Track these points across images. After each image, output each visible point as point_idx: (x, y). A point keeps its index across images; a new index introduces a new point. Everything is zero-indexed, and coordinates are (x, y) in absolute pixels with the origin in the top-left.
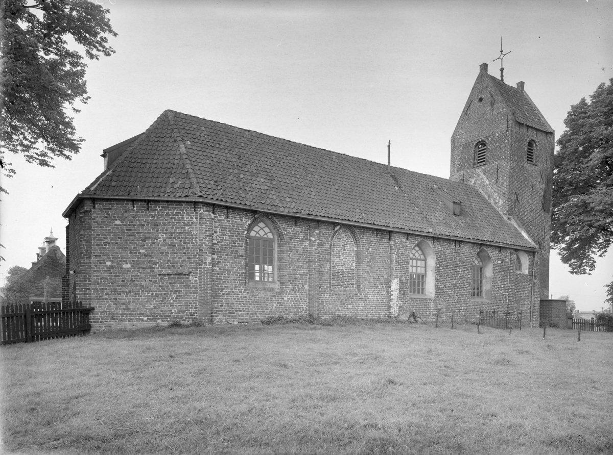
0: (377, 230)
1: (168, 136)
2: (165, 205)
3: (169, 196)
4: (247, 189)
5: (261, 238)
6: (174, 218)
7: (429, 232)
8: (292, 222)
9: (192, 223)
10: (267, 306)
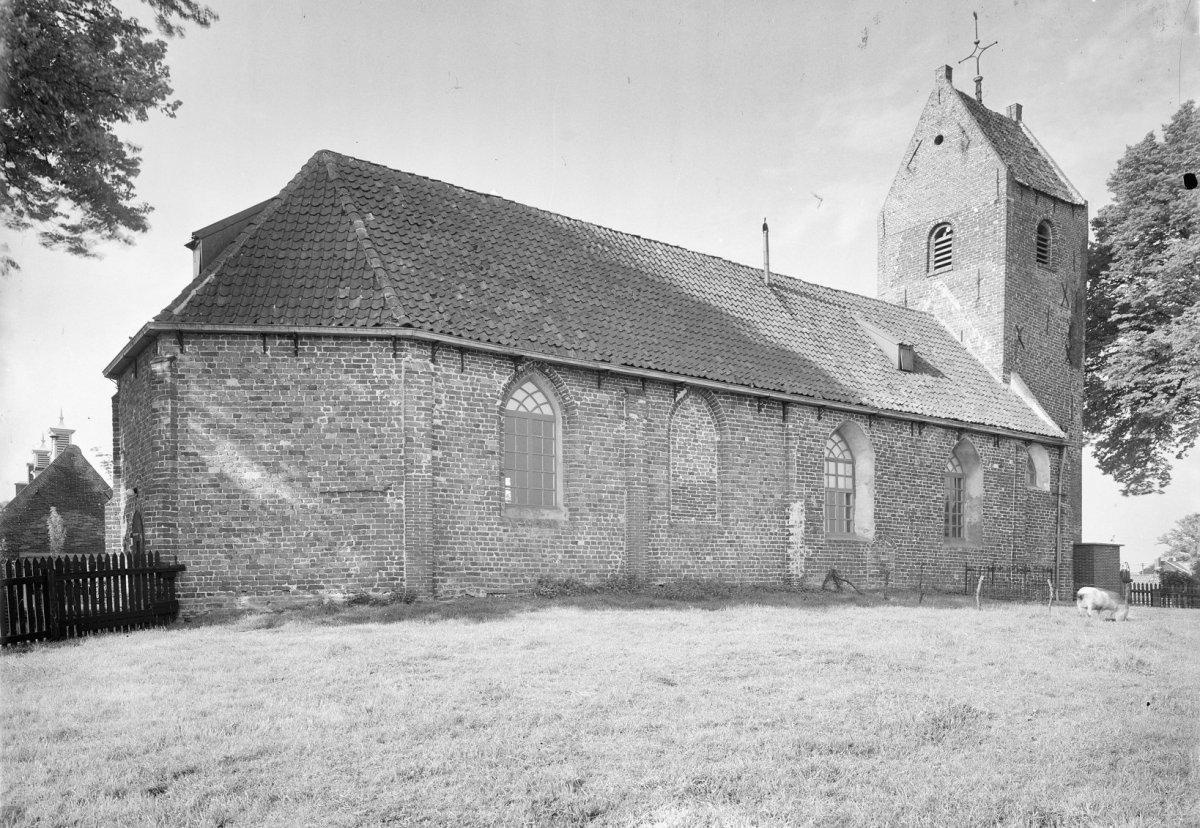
0: (759, 398)
1: (327, 203)
2: (332, 344)
3: (341, 324)
4: (498, 310)
5: (530, 413)
6: (351, 372)
7: (861, 404)
8: (591, 382)
9: (390, 382)
10: (544, 559)
